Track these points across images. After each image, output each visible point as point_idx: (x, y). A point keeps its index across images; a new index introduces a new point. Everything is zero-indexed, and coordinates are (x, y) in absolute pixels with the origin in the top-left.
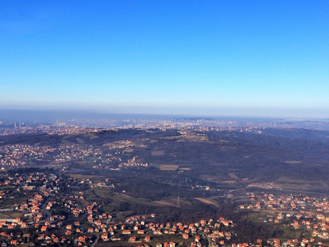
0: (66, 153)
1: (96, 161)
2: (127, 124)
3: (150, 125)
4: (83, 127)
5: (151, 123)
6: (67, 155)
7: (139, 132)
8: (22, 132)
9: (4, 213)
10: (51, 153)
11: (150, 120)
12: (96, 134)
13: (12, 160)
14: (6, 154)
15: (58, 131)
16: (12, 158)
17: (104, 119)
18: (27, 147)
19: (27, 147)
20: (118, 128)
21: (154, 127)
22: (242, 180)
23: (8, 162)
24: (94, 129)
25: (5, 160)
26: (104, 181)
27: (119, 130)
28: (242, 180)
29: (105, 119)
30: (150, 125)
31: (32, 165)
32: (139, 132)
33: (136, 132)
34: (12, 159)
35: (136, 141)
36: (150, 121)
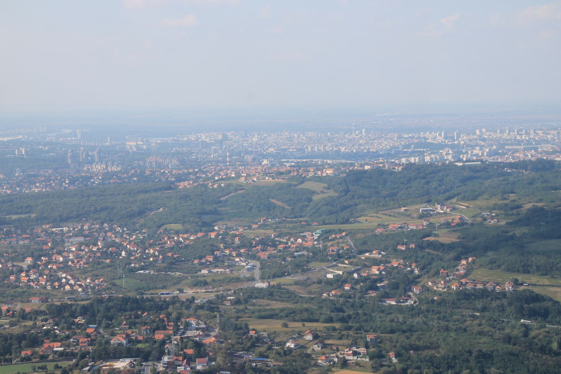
0: (234, 249)
1: (334, 276)
2: (435, 148)
3: (516, 147)
4: (287, 162)
5: (519, 143)
6: (239, 255)
7: (478, 174)
8: (94, 182)
9: (305, 315)
10: (187, 246)
11: (518, 131)
12: (329, 182)
13: (64, 275)
14: (44, 256)
15: (206, 175)
16: (65, 267)
17: (357, 132)
18: (111, 229)
19: (111, 229)
20: (404, 160)
21: (530, 156)
22: (359, 222)
23: (53, 278)
24: (321, 168)
25: (41, 275)
26: (361, 342)
27: (409, 166)
28: (359, 222)
29: (361, 133)
30: (516, 147)
31: (127, 287)
32: (478, 174)
33: (466, 174)
34: (59, 269)
35: (476, 178)
36: (518, 134)
